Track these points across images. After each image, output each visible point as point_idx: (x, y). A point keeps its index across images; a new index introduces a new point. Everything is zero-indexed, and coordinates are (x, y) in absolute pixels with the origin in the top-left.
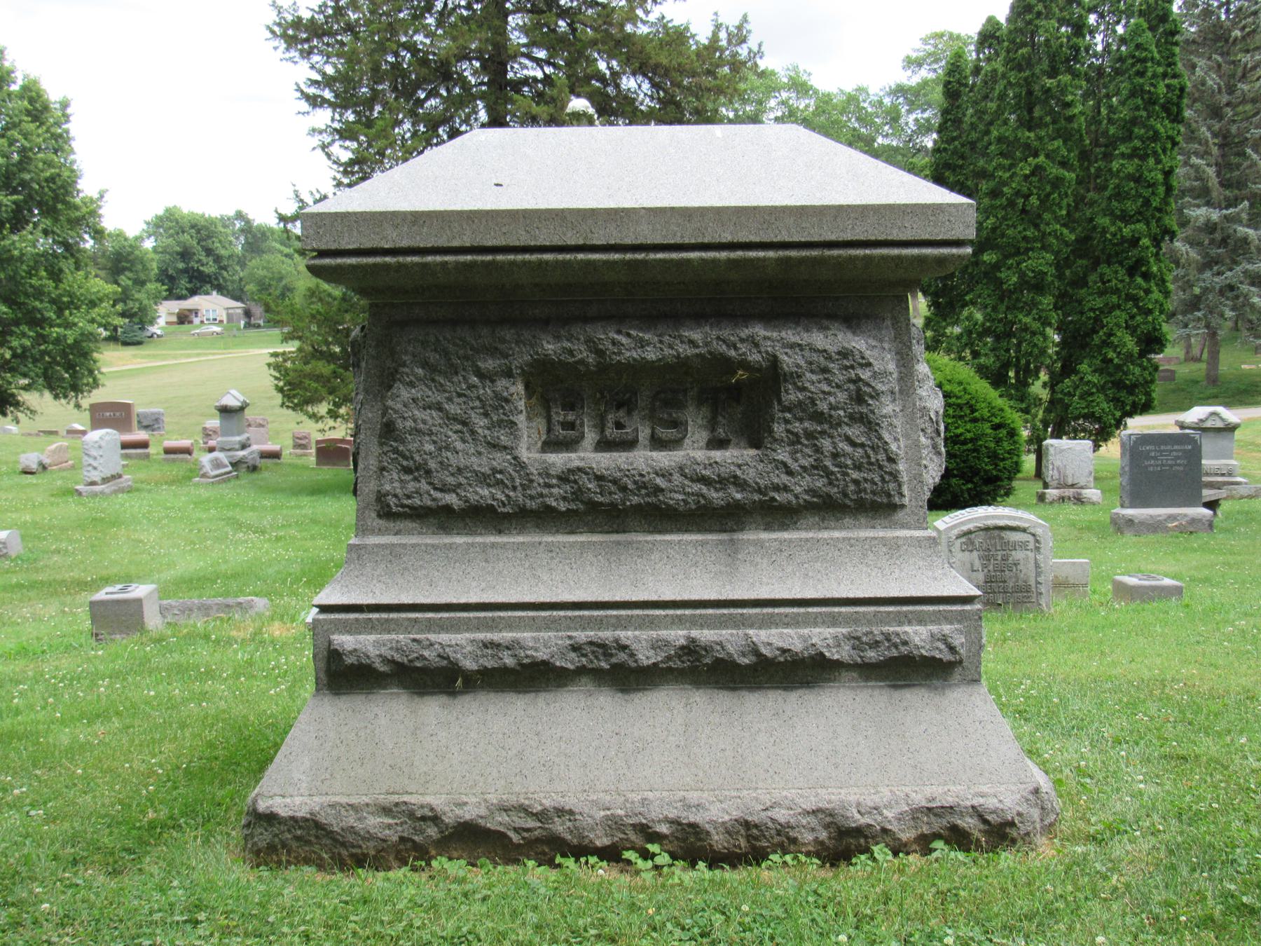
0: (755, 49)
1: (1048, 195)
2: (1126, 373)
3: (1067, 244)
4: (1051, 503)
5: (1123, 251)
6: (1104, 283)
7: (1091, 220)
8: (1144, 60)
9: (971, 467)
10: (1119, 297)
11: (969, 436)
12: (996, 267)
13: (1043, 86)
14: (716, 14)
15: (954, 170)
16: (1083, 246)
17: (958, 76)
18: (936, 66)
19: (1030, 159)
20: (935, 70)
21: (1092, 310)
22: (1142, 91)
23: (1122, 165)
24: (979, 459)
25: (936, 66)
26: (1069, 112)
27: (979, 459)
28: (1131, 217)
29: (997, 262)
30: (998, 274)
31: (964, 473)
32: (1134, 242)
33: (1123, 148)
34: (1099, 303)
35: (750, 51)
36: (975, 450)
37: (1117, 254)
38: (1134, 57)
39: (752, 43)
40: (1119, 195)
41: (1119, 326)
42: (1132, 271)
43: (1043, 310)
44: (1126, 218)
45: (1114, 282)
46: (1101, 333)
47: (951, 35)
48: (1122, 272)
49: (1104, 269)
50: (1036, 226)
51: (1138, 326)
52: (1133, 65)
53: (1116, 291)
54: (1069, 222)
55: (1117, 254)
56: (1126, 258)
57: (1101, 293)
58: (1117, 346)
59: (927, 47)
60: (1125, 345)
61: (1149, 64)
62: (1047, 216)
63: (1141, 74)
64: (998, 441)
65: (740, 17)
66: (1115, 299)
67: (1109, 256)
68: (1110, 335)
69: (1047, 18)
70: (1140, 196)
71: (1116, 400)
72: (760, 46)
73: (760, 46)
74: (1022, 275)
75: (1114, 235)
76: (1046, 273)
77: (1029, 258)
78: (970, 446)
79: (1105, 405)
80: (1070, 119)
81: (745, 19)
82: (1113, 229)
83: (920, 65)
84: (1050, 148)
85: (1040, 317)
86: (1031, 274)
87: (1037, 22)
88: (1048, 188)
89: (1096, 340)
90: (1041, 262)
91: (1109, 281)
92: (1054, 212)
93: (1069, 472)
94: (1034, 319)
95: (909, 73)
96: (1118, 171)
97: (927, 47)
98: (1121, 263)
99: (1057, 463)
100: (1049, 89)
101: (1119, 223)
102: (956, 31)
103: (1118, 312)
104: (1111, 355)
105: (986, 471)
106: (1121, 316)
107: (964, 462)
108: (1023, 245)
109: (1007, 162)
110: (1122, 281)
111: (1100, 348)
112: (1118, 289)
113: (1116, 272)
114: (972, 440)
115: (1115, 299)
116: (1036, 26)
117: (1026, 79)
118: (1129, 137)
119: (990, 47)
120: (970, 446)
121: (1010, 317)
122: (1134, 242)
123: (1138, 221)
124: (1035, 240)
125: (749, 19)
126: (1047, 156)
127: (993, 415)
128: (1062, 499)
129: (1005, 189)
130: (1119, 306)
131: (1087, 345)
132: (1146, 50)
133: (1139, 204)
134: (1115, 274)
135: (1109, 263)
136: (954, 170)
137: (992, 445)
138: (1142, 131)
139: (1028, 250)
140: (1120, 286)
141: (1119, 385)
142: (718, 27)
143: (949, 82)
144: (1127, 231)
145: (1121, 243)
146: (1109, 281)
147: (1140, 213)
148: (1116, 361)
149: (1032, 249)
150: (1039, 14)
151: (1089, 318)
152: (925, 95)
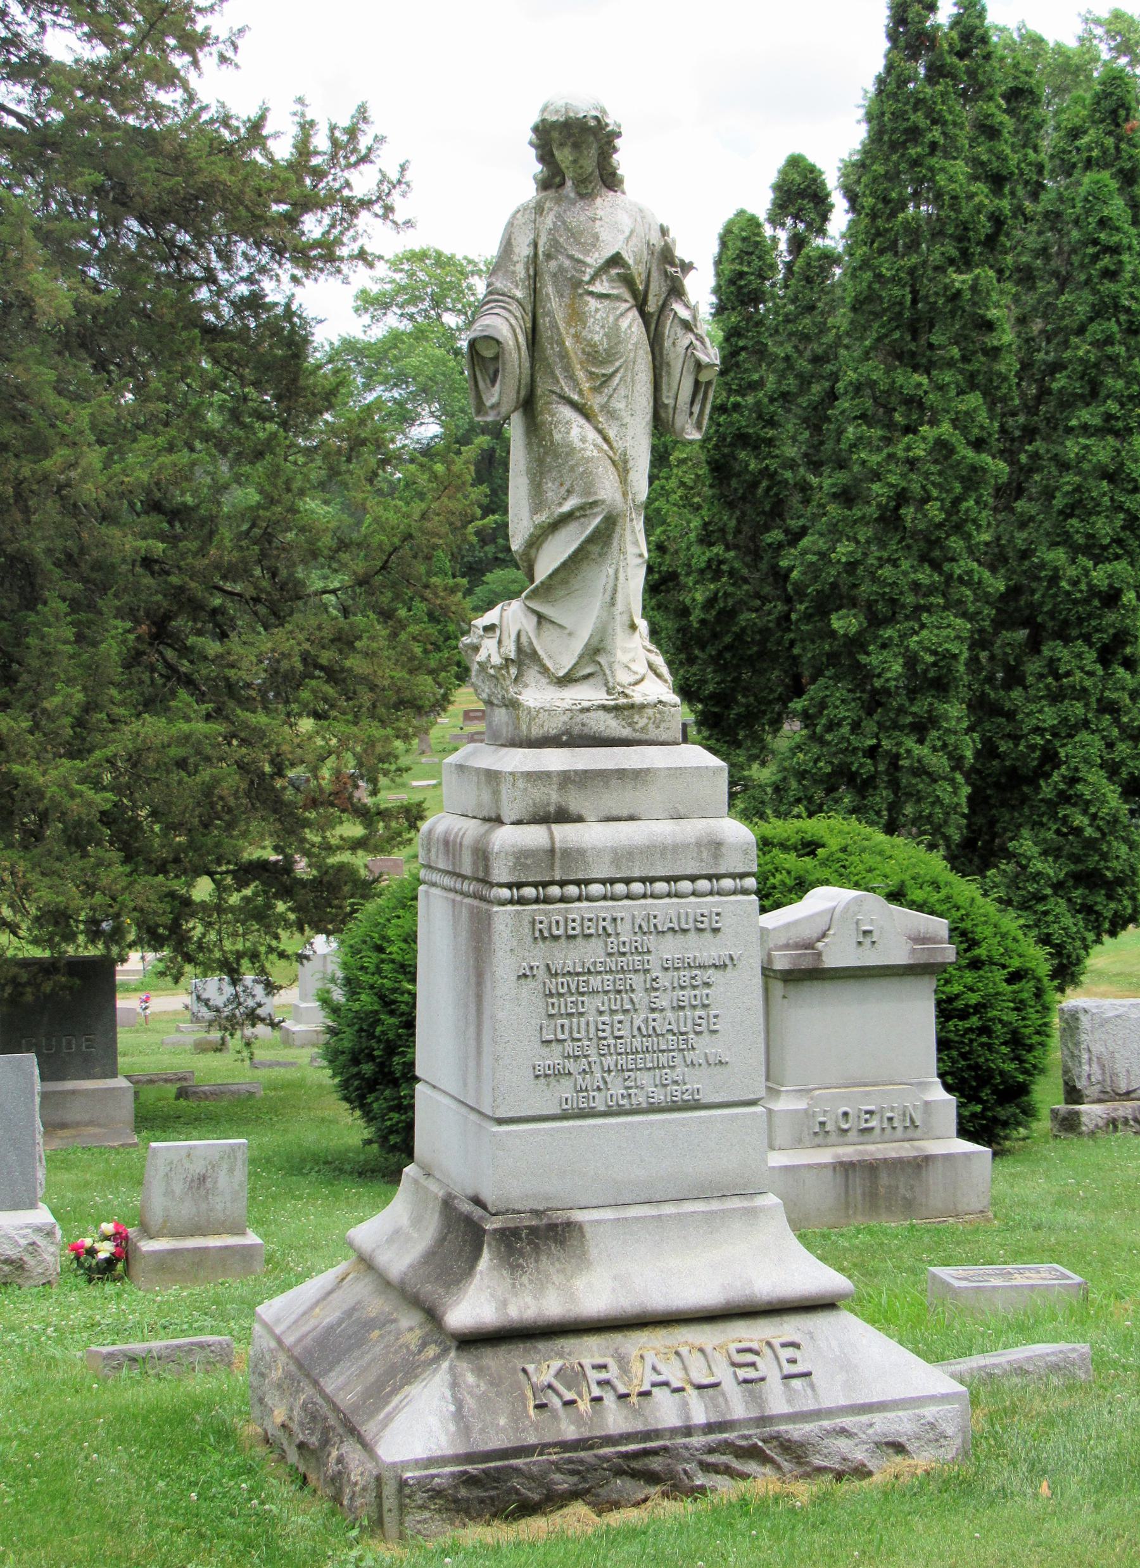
0: (394, 176)
1: (957, 502)
2: (1104, 857)
3: (987, 599)
4: (1092, 1134)
5: (1090, 616)
6: (1057, 677)
7: (1025, 555)
8: (1115, 250)
9: (976, 1067)
10: (1086, 705)
11: (974, 998)
12: (856, 643)
13: (946, 288)
14: (300, 101)
15: (756, 448)
16: (1012, 609)
17: (757, 263)
18: (413, 310)
19: (925, 429)
20: (411, 317)
21: (1037, 730)
22: (1116, 306)
23: (1086, 447)
24: (989, 1047)
25: (413, 310)
26: (992, 341)
27: (989, 1047)
28: (1105, 548)
29: (860, 633)
30: (863, 659)
31: (963, 1081)
32: (1112, 598)
33: (1086, 415)
34: (1049, 717)
35: (384, 178)
36: (985, 1030)
37: (1080, 620)
38: (1095, 242)
39: (387, 161)
40: (1077, 507)
41: (1086, 761)
42: (1106, 656)
43: (948, 731)
44: (1096, 551)
45: (1079, 675)
46: (1056, 777)
47: (439, 254)
48: (1090, 656)
49: (1053, 649)
50: (936, 566)
51: (1123, 762)
52: (1095, 258)
53: (1082, 694)
54: (996, 560)
55: (1080, 620)
56: (1097, 630)
57: (1055, 698)
58: (1088, 803)
59: (398, 276)
60: (1104, 801)
61: (1125, 257)
62: (956, 543)
63: (1111, 275)
64: (1020, 1007)
65: (353, 111)
66: (1078, 709)
67: (1066, 623)
68: (1073, 781)
69: (947, 156)
70: (1120, 508)
71: (1087, 910)
72: (403, 168)
73: (403, 168)
74: (911, 662)
75: (1075, 583)
76: (955, 657)
77: (923, 626)
78: (974, 1021)
79: (1068, 920)
80: (994, 353)
81: (362, 114)
82: (1072, 572)
83: (386, 307)
84: (963, 407)
85: (945, 746)
86: (930, 659)
87: (933, 161)
88: (958, 488)
89: (1047, 790)
90: (945, 634)
91: (1068, 674)
92: (968, 537)
93: (1120, 1067)
94: (934, 749)
95: (366, 319)
96: (1081, 459)
97: (398, 276)
98: (1087, 639)
99: (1097, 1048)
100: (958, 294)
101: (1085, 561)
102: (447, 251)
103: (1084, 736)
104: (1080, 820)
105: (1002, 1073)
106: (1090, 744)
107: (964, 1056)
108: (910, 599)
109: (877, 432)
110: (1090, 674)
111: (1052, 805)
112: (1084, 690)
113: (1079, 656)
114: (979, 1008)
115: (1078, 709)
116: (931, 169)
117: (912, 271)
118: (1094, 393)
119: (796, 217)
120: (974, 1021)
121: (886, 744)
122: (1112, 598)
123: (1117, 557)
124: (931, 590)
125: (371, 114)
126: (954, 422)
127: (1007, 952)
128: (1113, 1123)
129: (876, 487)
130: (1086, 724)
131: (1025, 799)
132: (1118, 229)
133: (1119, 523)
134: (1077, 660)
135: (1067, 640)
136: (756, 448)
137: (1013, 1017)
138: (1120, 384)
139: (918, 609)
140: (1088, 683)
141: (1090, 879)
142: (307, 128)
143: (741, 275)
144: (1100, 576)
145: (1087, 601)
146: (1068, 674)
147: (1119, 542)
148: (1089, 832)
149: (928, 609)
150: (934, 146)
151: (1032, 748)
152: (397, 359)
